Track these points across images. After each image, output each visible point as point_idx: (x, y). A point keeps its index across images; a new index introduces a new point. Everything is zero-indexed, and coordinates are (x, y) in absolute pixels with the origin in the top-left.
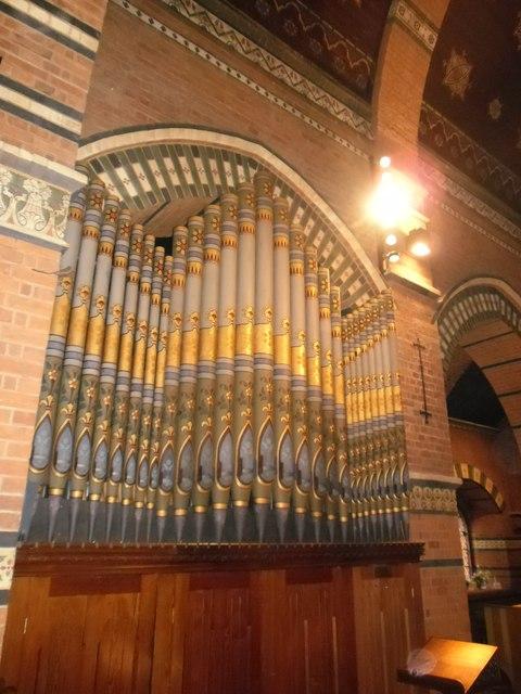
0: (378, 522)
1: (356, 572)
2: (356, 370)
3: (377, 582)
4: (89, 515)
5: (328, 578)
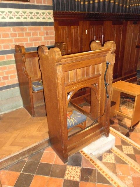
0: (136, 8)
1: (129, 22)
2: (77, 32)
3: (133, 25)
4: (64, 3)
5: (122, 24)
